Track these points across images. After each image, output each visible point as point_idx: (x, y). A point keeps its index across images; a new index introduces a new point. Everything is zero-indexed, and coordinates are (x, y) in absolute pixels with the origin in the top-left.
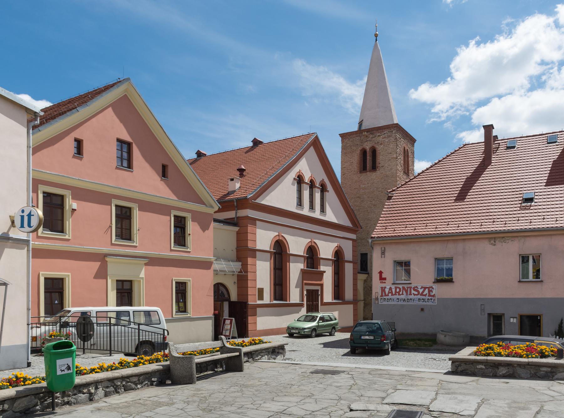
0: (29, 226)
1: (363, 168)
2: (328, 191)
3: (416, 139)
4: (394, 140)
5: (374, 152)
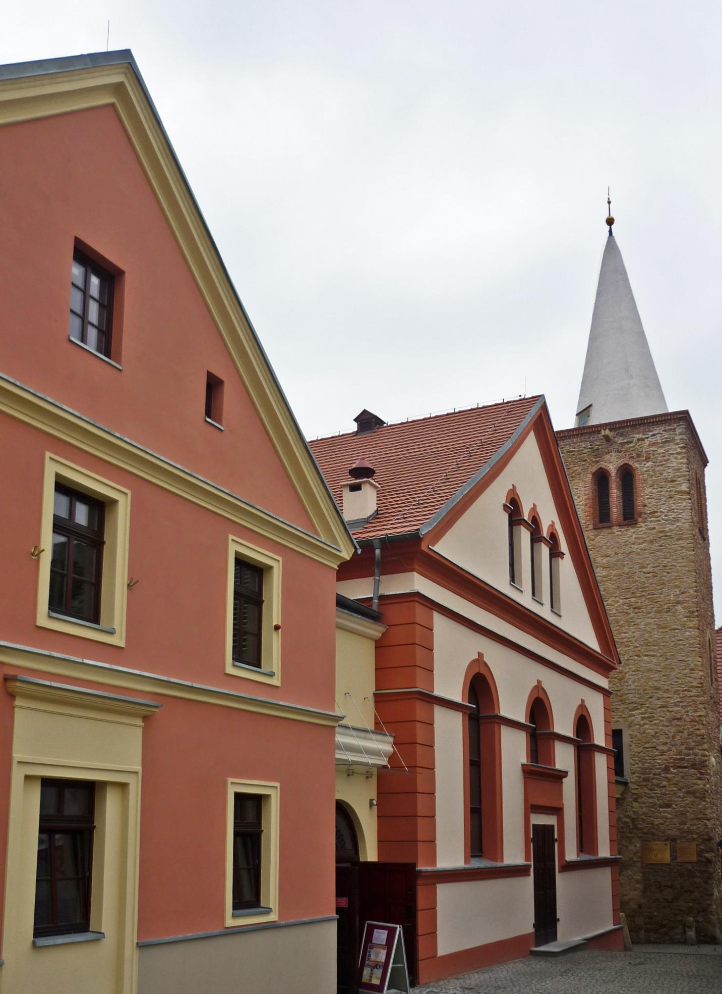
5: (627, 475)
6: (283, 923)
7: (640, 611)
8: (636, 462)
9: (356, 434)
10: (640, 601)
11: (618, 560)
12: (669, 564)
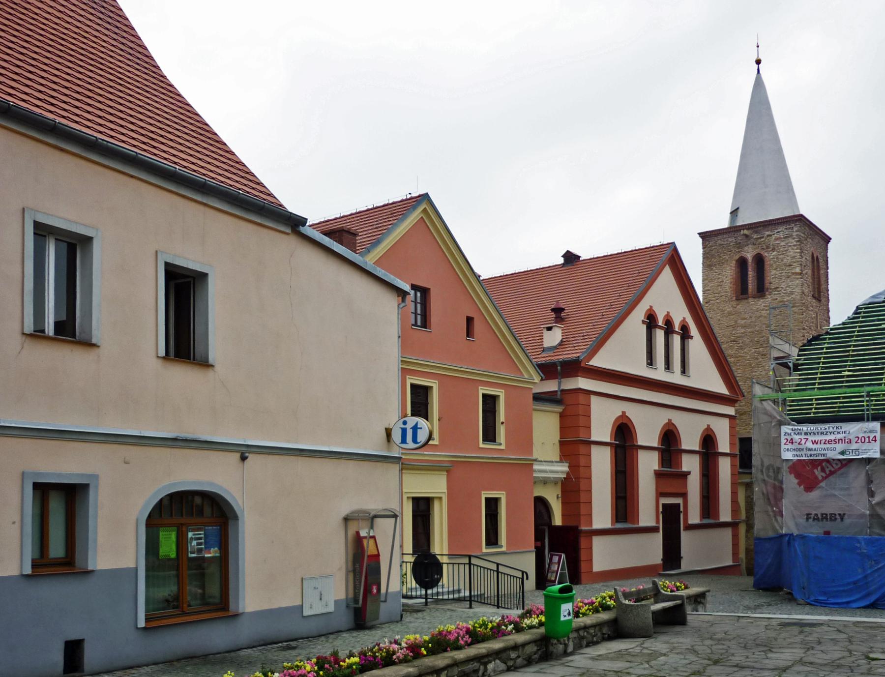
0: (415, 440)
1: (742, 291)
2: (692, 337)
3: (831, 237)
4: (795, 243)
5: (760, 260)
6: (508, 552)
7: (766, 357)
8: (766, 252)
9: (563, 265)
10: (765, 350)
11: (751, 322)
12: (786, 324)
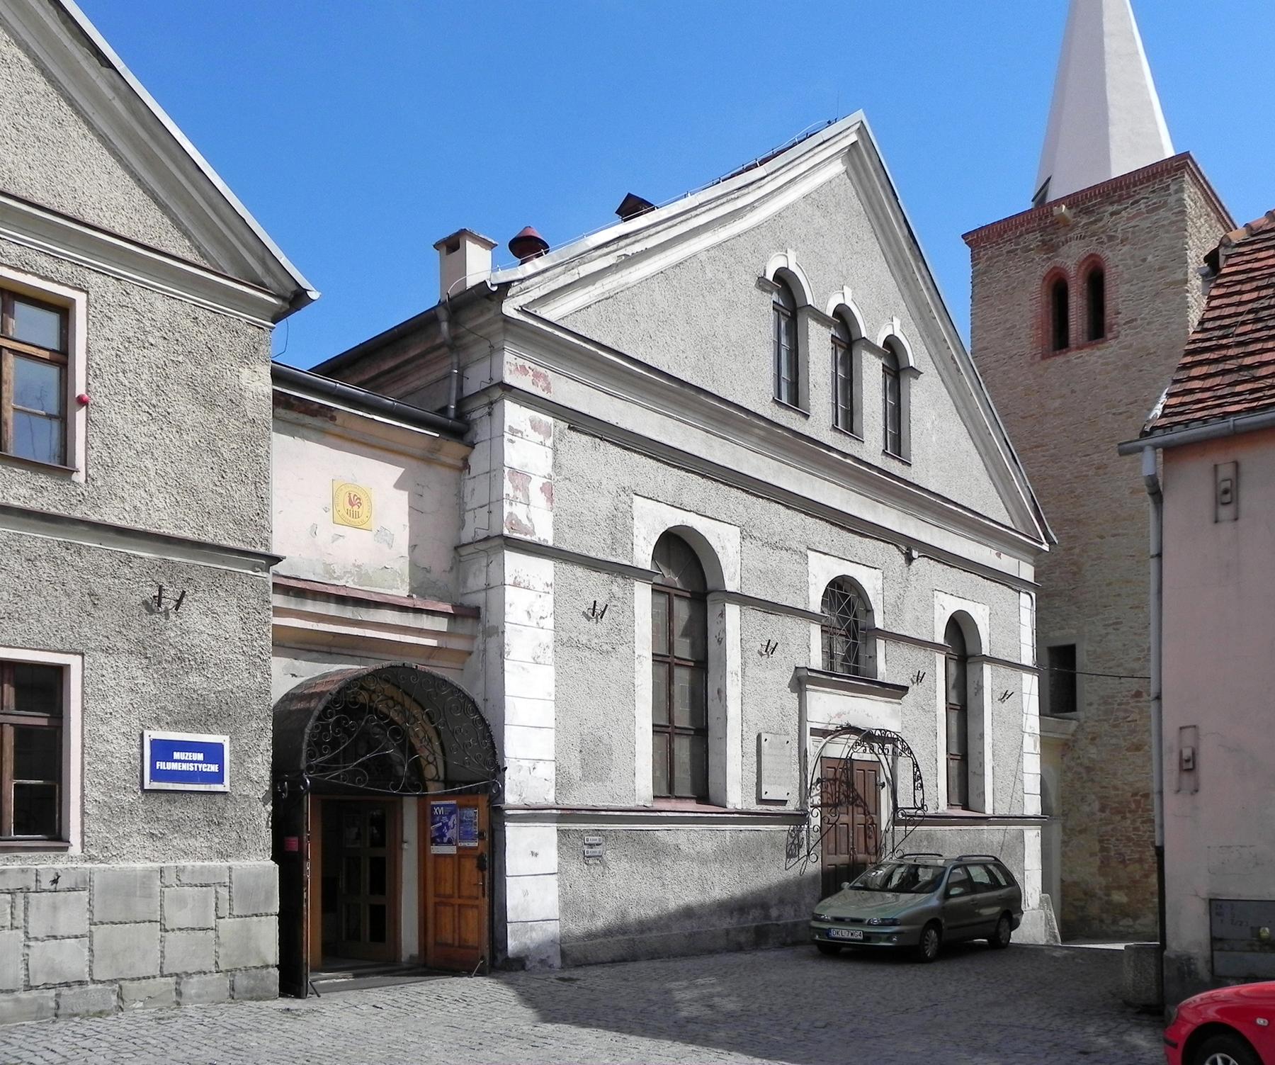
2: (916, 373)
5: (1096, 280)
